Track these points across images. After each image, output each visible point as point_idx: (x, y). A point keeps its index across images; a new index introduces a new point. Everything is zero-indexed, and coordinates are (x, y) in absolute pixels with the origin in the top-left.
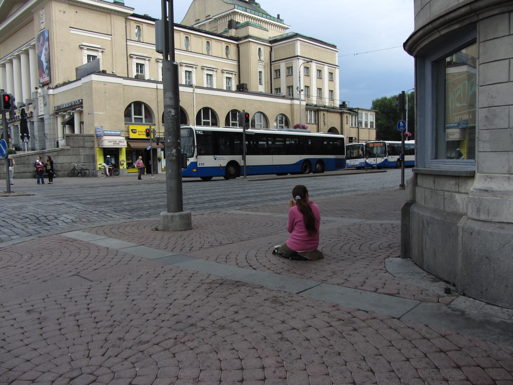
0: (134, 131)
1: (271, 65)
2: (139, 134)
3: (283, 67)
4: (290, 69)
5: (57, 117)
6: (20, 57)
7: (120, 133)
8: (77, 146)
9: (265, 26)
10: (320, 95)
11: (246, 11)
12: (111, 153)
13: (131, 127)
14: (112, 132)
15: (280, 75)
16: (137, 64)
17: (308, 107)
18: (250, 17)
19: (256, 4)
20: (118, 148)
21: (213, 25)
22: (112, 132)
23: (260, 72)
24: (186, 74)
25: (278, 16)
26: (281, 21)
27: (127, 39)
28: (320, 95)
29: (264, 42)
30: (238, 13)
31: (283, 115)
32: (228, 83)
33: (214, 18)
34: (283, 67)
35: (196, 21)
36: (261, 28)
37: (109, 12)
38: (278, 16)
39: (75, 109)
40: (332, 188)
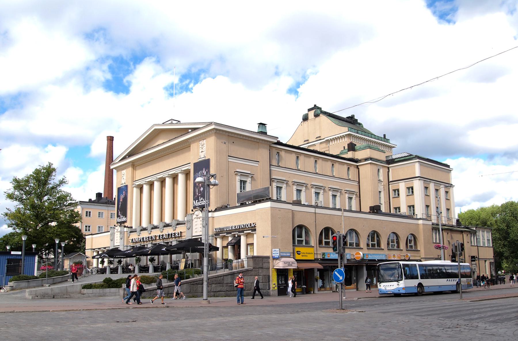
0: (299, 253)
1: (389, 184)
2: (302, 256)
3: (402, 187)
4: (411, 189)
5: (216, 238)
6: (457, 224)
7: (289, 254)
8: (258, 267)
9: (381, 148)
10: (439, 213)
11: (358, 133)
12: (282, 273)
13: (297, 249)
14: (284, 254)
15: (399, 195)
16: (241, 181)
17: (434, 226)
18: (371, 141)
19: (360, 124)
20: (288, 269)
21: (324, 145)
22: (284, 254)
23: (380, 192)
24: (241, 184)
25: (385, 135)
26: (387, 141)
27: (270, 165)
28: (439, 213)
29: (382, 163)
30: (352, 135)
31: (412, 234)
32: (350, 203)
33: (326, 139)
34: (402, 187)
35: (305, 141)
36: (379, 150)
37: (258, 141)
38: (385, 135)
39: (243, 232)
40: (503, 306)
